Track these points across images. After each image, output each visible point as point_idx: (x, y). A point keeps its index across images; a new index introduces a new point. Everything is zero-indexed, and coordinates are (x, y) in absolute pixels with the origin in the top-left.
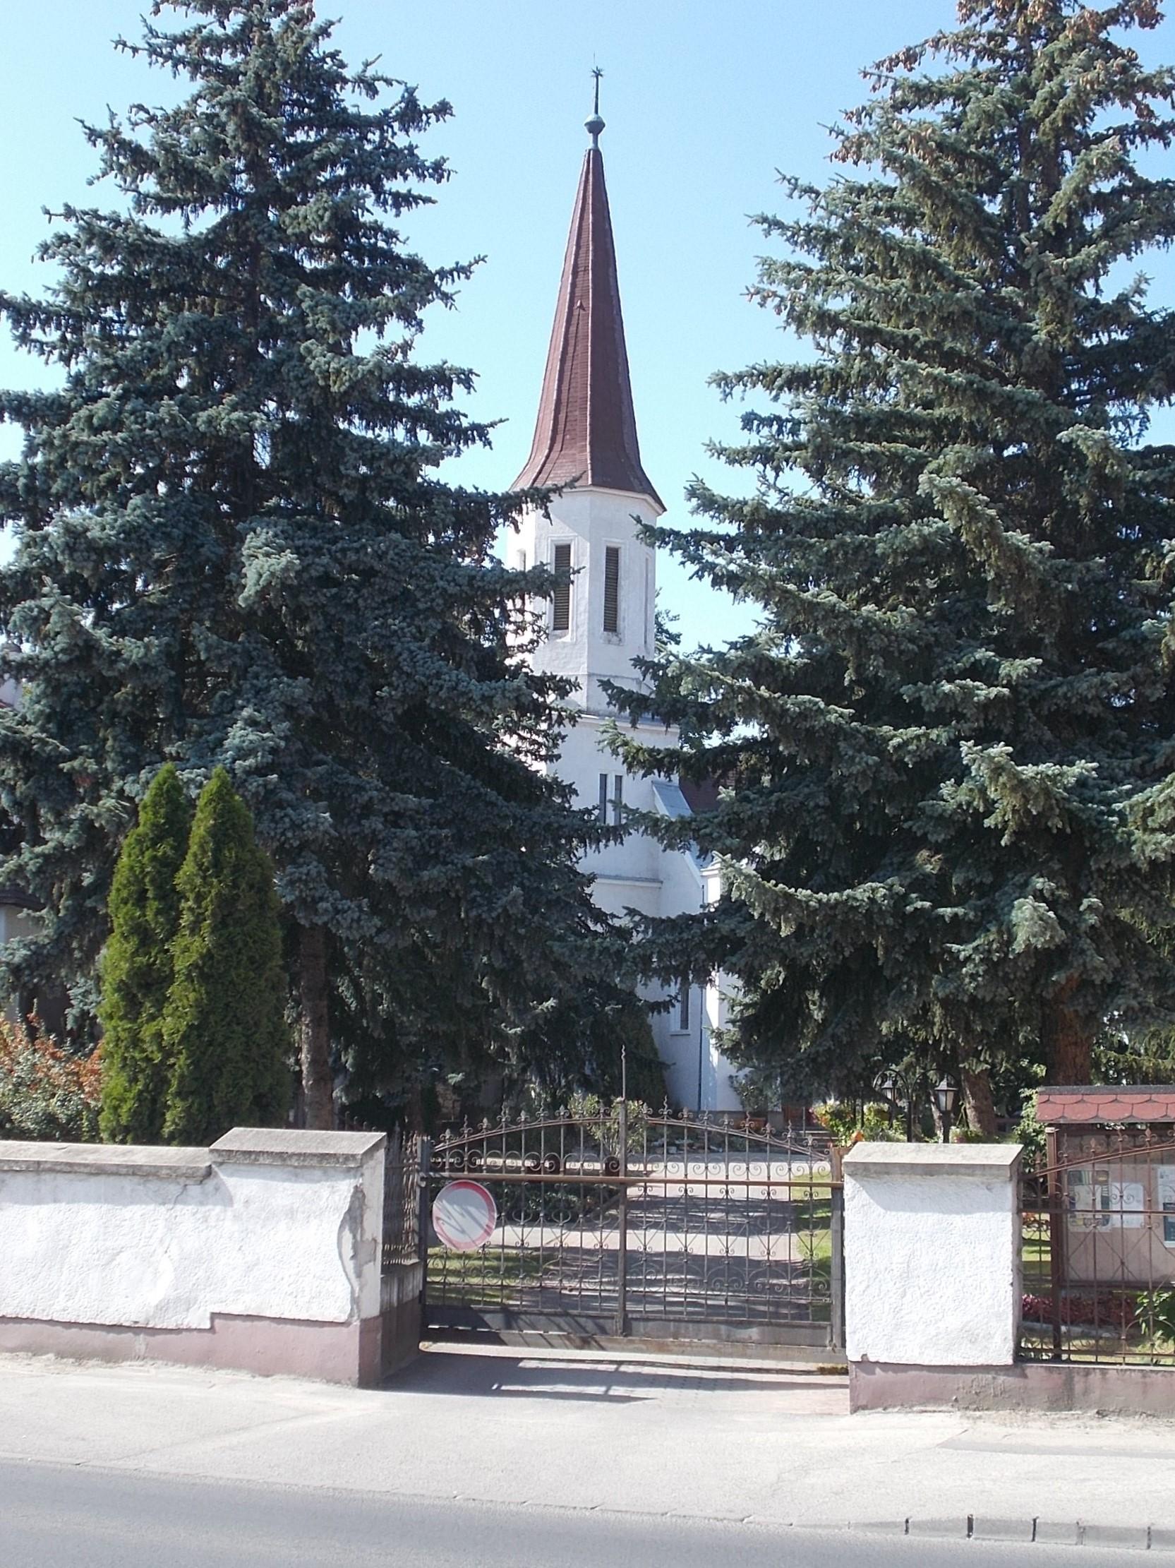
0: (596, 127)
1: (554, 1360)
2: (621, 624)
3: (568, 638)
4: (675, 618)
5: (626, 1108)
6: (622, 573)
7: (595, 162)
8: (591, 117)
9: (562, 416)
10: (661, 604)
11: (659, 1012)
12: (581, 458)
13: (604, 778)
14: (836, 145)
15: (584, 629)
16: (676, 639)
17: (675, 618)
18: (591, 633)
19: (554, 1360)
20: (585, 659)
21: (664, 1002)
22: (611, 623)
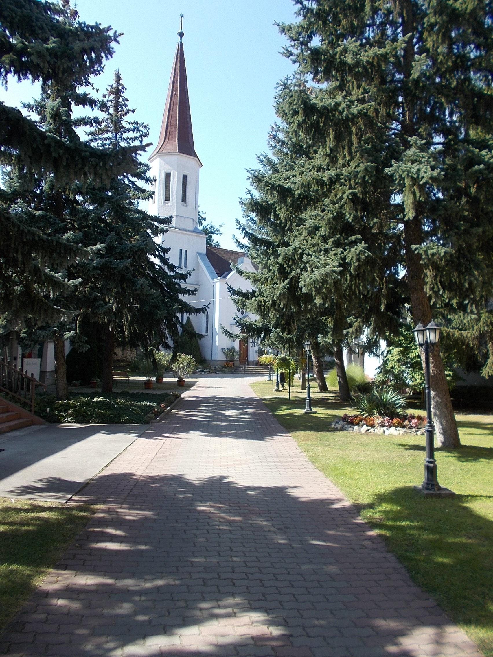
0: (181, 35)
1: (186, 259)
2: (187, 200)
3: (169, 204)
4: (205, 213)
5: (185, 358)
6: (188, 183)
7: (181, 47)
8: (180, 31)
9: (168, 130)
10: (200, 209)
11: (200, 313)
12: (175, 143)
13: (181, 250)
14: (274, 23)
15: (175, 200)
16: (204, 219)
17: (205, 213)
18: (177, 202)
19: (186, 259)
20: (175, 210)
21: (202, 308)
22: (184, 200)
